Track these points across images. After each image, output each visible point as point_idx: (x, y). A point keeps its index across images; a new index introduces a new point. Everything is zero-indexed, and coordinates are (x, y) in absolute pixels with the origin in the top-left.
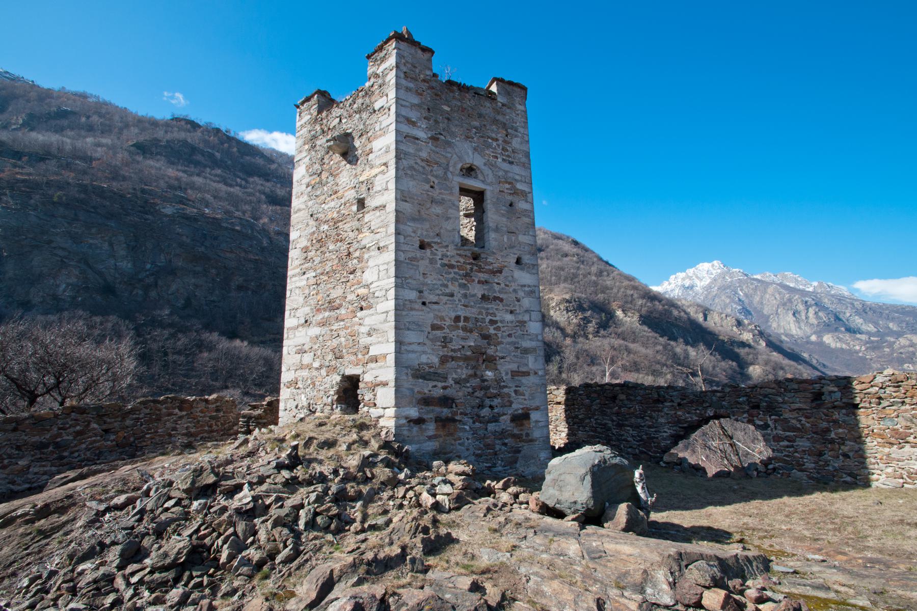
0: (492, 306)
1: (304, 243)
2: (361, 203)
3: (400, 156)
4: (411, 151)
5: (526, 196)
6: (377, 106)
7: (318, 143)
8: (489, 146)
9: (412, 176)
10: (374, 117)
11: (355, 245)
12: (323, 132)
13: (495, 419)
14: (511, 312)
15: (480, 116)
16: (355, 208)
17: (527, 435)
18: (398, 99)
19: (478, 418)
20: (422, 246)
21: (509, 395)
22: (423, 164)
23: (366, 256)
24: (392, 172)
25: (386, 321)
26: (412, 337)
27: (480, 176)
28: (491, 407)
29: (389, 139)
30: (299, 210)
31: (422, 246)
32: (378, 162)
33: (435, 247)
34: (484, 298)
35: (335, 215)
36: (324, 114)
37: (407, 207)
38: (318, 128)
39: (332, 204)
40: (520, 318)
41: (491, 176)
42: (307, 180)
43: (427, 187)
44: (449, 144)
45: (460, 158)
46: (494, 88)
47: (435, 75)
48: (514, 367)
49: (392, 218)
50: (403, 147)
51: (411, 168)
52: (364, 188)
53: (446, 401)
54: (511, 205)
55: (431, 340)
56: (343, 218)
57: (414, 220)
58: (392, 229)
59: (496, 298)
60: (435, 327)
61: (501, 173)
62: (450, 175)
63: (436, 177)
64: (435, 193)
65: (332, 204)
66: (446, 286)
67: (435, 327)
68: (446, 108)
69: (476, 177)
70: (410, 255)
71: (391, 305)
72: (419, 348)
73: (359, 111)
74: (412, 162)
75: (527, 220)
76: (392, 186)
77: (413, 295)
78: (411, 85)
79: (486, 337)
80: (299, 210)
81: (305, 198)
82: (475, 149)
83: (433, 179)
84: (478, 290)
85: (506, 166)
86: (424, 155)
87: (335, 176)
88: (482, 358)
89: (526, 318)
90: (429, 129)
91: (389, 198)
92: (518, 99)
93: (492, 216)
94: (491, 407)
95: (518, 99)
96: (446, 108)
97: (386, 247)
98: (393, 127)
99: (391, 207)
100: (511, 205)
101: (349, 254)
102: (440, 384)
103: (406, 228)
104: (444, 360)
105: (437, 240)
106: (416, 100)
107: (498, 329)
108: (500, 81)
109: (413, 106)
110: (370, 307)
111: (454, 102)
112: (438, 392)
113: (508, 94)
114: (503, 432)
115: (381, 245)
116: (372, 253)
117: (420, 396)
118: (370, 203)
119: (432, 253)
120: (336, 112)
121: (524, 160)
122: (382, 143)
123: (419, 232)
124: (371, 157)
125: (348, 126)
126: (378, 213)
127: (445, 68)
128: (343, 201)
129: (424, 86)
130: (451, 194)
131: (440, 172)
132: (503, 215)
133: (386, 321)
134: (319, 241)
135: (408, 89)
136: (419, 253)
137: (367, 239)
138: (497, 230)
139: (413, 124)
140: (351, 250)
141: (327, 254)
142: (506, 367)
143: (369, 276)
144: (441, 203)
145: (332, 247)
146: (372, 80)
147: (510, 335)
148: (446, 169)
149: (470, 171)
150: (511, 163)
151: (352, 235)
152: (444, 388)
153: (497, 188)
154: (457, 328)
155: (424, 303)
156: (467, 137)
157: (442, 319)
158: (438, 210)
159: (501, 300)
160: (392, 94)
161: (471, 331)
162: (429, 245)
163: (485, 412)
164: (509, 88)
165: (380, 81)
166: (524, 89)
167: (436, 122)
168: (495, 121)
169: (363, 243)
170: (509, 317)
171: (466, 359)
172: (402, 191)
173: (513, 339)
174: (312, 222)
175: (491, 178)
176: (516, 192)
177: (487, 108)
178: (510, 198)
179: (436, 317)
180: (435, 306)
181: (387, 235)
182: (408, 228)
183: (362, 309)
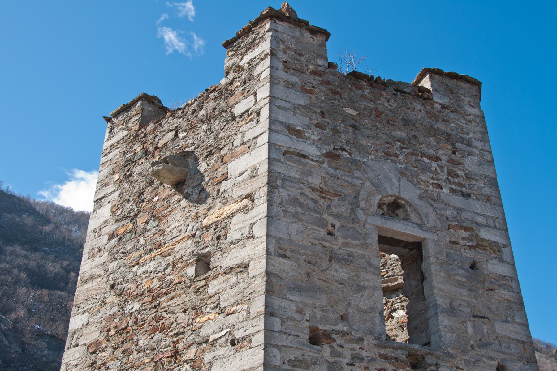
1: (93, 335)
2: (203, 263)
3: (272, 185)
4: (294, 174)
5: (500, 251)
6: (238, 110)
7: (137, 169)
8: (425, 169)
9: (295, 215)
10: (233, 126)
11: (189, 338)
12: (146, 153)
15: (407, 122)
16: (191, 271)
18: (272, 98)
20: (315, 339)
22: (315, 195)
24: (261, 208)
27: (413, 217)
29: (260, 156)
30: (92, 278)
31: (315, 339)
32: (237, 193)
33: (339, 340)
35: (155, 284)
36: (150, 127)
37: (284, 266)
38: (138, 148)
39: (152, 266)
41: (432, 216)
43: (322, 233)
45: (378, 187)
46: (426, 83)
47: (331, 65)
49: (260, 285)
50: (280, 169)
51: (294, 201)
52: (209, 236)
54: (473, 266)
56: (169, 288)
57: (298, 289)
58: (259, 306)
61: (449, 212)
62: (361, 215)
63: (338, 217)
64: (336, 244)
65: (152, 266)
68: (351, 111)
69: (407, 219)
70: (293, 355)
73: (208, 119)
74: (295, 193)
75: (507, 294)
76: (261, 230)
78: (294, 79)
80: (92, 278)
81: (105, 256)
82: (402, 173)
83: (331, 220)
85: (457, 201)
86: (316, 181)
87: (160, 220)
90: (323, 141)
91: (255, 253)
92: (467, 99)
93: (441, 286)
95: (467, 99)
96: (351, 111)
97: (247, 338)
98: (265, 138)
99: (259, 267)
100: (473, 266)
101: (176, 354)
105: (341, 327)
106: (302, 100)
108: (435, 73)
109: (296, 108)
111: (364, 103)
113: (451, 91)
115: (238, 335)
116: (220, 352)
117: (476, 262)
118: (222, 261)
119: (334, 353)
120: (169, 123)
121: (487, 190)
122: (248, 163)
123: (308, 313)
124: (224, 186)
125: (187, 142)
126: (233, 279)
127: (345, 56)
128: (171, 259)
129: (315, 80)
130: (364, 246)
131: (344, 209)
132: (460, 285)
134: (120, 331)
135: (289, 85)
136: (309, 352)
137: (211, 325)
138: (452, 311)
139: (298, 134)
140: (180, 346)
141: (134, 356)
144: (347, 260)
145: (143, 341)
146: (232, 75)
148: (355, 203)
149: (394, 208)
150: (467, 196)
151: (182, 318)
156: (388, 155)
158: (341, 272)
160: (264, 92)
162: (328, 336)
164: (452, 83)
165: (244, 75)
166: (477, 84)
167: (335, 131)
168: (431, 131)
169: (204, 332)
172: (279, 240)
174: (112, 298)
175: (432, 220)
176: (480, 245)
178: (470, 254)
181: (249, 317)
182: (288, 304)
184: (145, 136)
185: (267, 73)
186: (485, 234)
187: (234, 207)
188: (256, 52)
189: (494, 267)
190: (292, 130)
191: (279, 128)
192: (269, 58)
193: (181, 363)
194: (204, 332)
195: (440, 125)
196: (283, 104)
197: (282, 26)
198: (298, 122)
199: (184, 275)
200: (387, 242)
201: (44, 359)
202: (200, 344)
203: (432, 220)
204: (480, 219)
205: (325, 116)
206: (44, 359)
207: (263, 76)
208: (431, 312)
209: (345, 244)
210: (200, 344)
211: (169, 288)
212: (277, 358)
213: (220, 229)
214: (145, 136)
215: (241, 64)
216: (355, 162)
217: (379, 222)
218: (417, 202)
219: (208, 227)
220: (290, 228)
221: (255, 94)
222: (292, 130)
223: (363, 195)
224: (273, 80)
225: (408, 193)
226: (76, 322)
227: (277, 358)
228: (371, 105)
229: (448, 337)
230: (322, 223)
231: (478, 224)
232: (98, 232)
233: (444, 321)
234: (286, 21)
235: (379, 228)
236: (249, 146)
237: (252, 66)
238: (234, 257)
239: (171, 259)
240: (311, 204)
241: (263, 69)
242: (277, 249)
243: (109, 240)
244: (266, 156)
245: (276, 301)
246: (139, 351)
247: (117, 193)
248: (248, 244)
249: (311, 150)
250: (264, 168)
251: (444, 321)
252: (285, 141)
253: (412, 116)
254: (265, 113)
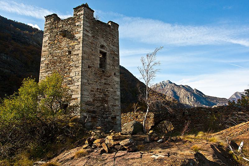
0: (107, 86)
2: (70, 52)
6: (77, 24)
8: (108, 40)
13: (107, 118)
14: (112, 88)
15: (106, 31)
16: (67, 53)
17: (115, 123)
19: (102, 117)
21: (111, 112)
23: (71, 69)
25: (78, 88)
26: (85, 93)
27: (105, 49)
28: (106, 114)
31: (89, 67)
34: (105, 84)
40: (115, 90)
42: (48, 42)
44: (98, 39)
46: (110, 24)
48: (112, 104)
53: (94, 112)
55: (91, 94)
57: (87, 59)
58: (80, 61)
59: (108, 84)
60: (92, 91)
61: (111, 48)
64: (93, 52)
66: (95, 79)
67: (92, 91)
71: (80, 83)
72: (87, 97)
76: (81, 49)
77: (86, 81)
79: (105, 95)
84: (103, 81)
85: (112, 46)
86: (90, 41)
88: (104, 101)
89: (116, 90)
91: (80, 52)
94: (106, 114)
98: (82, 31)
99: (80, 55)
101: (65, 67)
102: (92, 107)
103: (84, 61)
104: (94, 100)
107: (108, 93)
110: (72, 84)
112: (92, 109)
114: (109, 121)
132: (111, 60)
133: (78, 88)
135: (87, 21)
138: (109, 64)
139: (88, 32)
140: (66, 66)
142: (110, 103)
143: (72, 74)
144: (95, 55)
147: (112, 95)
149: (102, 46)
150: (114, 46)
152: (94, 108)
153: (109, 52)
154: (98, 91)
155: (89, 84)
156: (102, 37)
157: (94, 89)
158: (93, 57)
159: (110, 85)
160: (82, 22)
161: (101, 93)
163: (104, 116)
168: (110, 33)
169: (70, 64)
170: (111, 90)
171: (100, 100)
172: (84, 51)
173: (112, 96)
175: (108, 50)
177: (108, 29)
179: (92, 88)
180: (92, 85)
182: (85, 62)
183: (69, 84)
184: (55, 24)
185: (82, 18)
186: (116, 53)
187: (76, 43)
188: (80, 13)
189: (116, 58)
190: (87, 31)
191: (85, 30)
192: (83, 15)
193: (173, 85)
194: (70, 64)
195: (111, 32)
196: (85, 25)
197: (86, 8)
198: (88, 29)
199: (66, 54)
200: (101, 52)
201: (3, 59)
202: (70, 66)
203: (108, 50)
204: (115, 50)
205: (93, 29)
206: (3, 59)
207: (82, 19)
208: (106, 64)
209: (94, 52)
210: (70, 66)
211: (63, 56)
212: (83, 70)
213: (73, 47)
214: (55, 24)
215: (77, 14)
216: (97, 38)
217: (100, 49)
218: (106, 46)
219: (70, 46)
220: (86, 49)
221: (80, 22)
222: (87, 31)
223: (98, 44)
224: (84, 20)
225: (105, 44)
226: (42, 59)
227: (83, 70)
228: (100, 27)
229: (108, 68)
230: (91, 49)
231: (115, 51)
232: (46, 42)
233: (108, 66)
234: (154, 147)
235: (100, 50)
236: (79, 32)
237: (80, 15)
238: (76, 53)
239: (63, 50)
240: (89, 45)
241: (82, 17)
242: (84, 52)
243: (48, 44)
244: (82, 35)
245: (83, 61)
246: (57, 66)
247: (49, 35)
248: (79, 49)
249: (90, 35)
250: (82, 37)
251: (108, 66)
252: (85, 32)
253: (107, 30)
254: (82, 26)
